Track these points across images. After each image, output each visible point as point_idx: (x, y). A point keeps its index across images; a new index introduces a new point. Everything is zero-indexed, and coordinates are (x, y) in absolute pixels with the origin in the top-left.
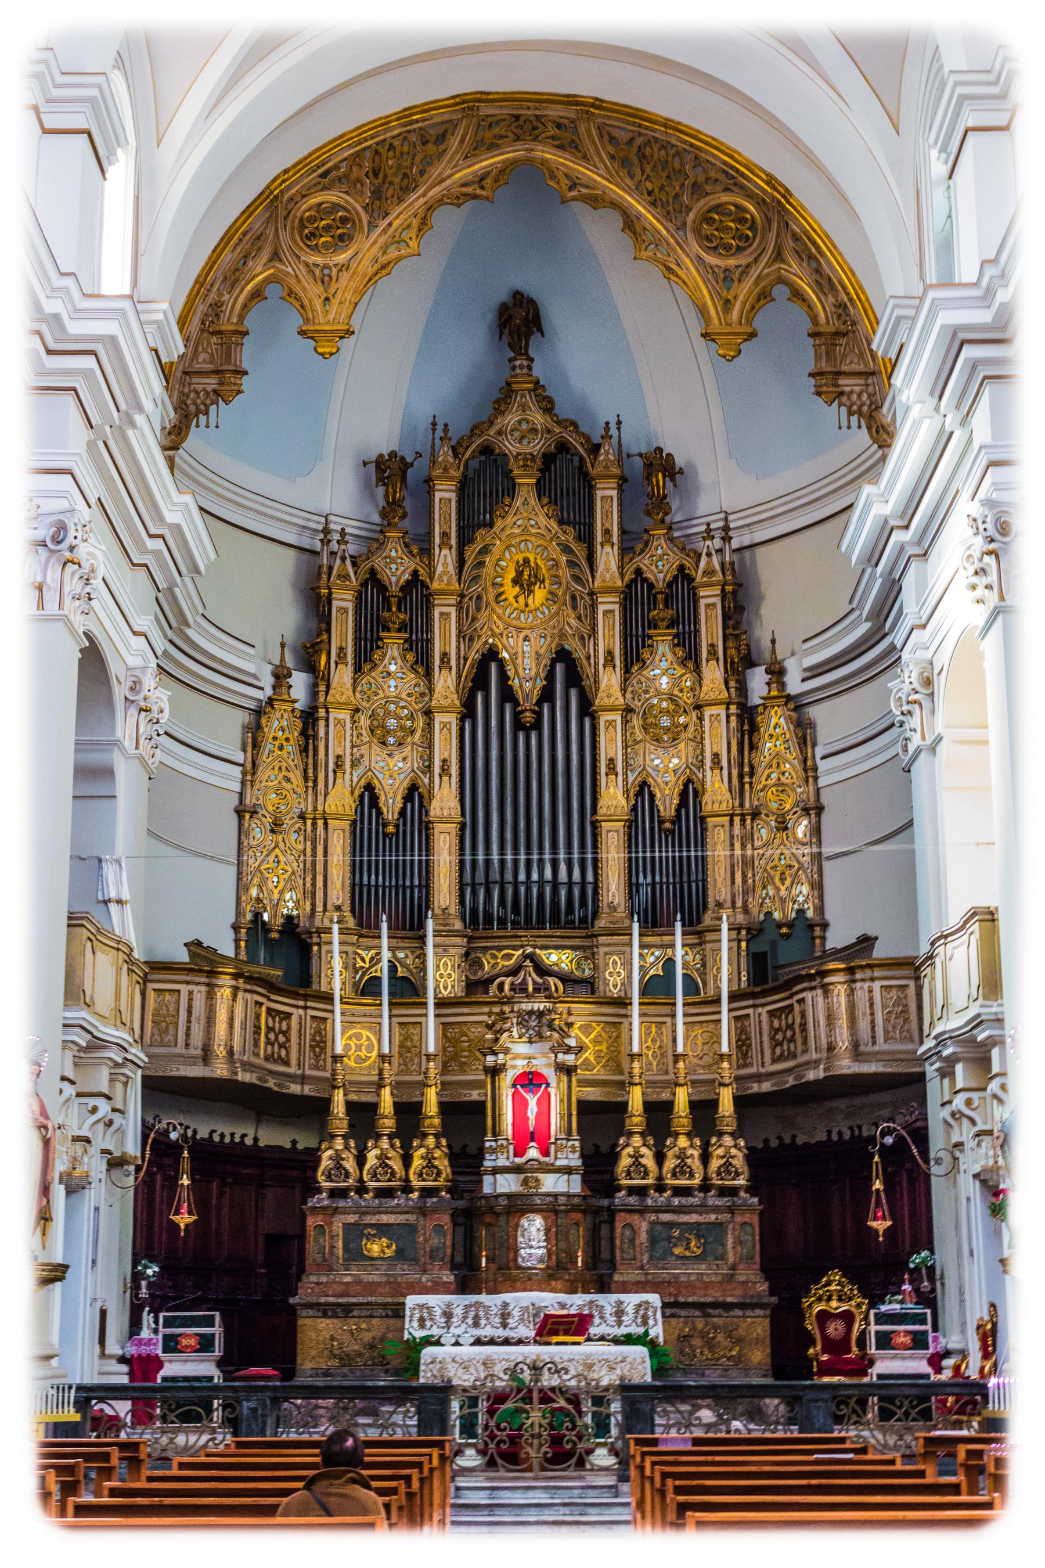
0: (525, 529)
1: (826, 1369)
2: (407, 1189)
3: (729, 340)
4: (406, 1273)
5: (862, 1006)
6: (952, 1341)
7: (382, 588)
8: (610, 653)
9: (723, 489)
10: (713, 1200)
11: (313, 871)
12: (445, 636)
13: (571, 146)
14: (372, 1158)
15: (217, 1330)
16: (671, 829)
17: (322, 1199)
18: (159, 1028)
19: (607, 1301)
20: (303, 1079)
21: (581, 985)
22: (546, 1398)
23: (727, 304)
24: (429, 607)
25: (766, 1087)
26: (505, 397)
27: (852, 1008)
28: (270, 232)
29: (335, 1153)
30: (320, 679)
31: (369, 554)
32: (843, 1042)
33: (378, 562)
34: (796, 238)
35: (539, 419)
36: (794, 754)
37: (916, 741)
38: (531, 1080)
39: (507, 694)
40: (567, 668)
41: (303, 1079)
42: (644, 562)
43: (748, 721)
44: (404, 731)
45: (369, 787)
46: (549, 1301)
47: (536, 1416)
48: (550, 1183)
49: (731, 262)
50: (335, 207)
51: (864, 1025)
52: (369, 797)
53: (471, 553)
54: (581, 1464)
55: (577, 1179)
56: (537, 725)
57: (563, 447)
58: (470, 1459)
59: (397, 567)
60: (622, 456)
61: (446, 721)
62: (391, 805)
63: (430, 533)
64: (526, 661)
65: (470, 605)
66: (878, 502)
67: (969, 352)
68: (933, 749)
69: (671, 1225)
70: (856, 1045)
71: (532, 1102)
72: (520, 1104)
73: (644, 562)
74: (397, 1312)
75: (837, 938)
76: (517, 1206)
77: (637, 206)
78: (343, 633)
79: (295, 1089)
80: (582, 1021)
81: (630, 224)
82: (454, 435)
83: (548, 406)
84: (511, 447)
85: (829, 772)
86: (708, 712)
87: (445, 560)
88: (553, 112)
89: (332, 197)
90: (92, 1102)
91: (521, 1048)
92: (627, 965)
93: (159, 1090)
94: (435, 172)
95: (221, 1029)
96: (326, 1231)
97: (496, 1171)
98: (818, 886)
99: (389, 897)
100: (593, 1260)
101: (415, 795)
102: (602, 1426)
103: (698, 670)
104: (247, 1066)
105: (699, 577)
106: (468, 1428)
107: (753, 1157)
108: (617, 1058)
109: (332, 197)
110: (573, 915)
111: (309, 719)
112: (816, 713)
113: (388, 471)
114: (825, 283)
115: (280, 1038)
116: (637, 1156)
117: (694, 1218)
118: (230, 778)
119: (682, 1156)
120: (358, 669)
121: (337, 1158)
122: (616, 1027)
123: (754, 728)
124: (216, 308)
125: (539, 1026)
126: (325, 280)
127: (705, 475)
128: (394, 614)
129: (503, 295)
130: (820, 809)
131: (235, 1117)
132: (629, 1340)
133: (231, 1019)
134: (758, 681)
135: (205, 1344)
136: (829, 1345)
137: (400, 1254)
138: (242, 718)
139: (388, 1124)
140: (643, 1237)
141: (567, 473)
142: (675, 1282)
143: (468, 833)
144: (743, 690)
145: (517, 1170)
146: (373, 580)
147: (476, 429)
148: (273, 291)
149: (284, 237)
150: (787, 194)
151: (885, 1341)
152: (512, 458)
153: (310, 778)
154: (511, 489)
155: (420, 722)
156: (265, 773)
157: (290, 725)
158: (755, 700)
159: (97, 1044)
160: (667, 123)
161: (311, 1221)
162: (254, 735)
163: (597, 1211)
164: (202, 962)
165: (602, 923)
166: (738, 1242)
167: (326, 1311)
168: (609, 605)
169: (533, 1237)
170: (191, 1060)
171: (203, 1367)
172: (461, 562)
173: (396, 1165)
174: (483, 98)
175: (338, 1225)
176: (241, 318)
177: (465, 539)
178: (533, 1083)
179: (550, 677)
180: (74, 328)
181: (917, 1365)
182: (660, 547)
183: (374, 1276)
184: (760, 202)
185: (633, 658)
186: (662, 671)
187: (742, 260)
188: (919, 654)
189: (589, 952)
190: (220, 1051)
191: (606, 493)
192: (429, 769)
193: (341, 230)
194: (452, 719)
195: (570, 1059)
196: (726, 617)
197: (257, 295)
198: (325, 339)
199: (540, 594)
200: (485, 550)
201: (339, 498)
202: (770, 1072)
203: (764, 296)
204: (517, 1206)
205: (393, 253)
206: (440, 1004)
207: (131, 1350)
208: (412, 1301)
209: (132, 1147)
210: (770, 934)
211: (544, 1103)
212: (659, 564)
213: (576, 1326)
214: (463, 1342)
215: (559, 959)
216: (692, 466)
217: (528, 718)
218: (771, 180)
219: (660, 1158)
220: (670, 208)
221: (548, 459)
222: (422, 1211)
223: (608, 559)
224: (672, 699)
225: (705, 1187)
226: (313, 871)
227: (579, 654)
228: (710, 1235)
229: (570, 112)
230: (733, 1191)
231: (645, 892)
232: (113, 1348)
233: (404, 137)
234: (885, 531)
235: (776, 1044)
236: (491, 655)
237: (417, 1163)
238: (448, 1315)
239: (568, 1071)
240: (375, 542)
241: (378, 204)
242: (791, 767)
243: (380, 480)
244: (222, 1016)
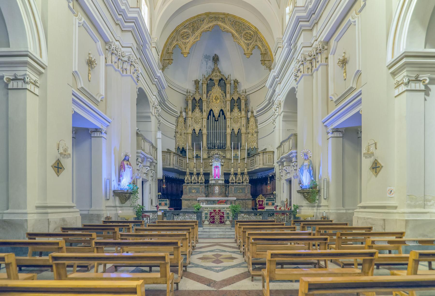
0: (216, 91)
1: (259, 209)
2: (198, 183)
3: (248, 55)
6: (279, 204)
8: (228, 110)
9: (245, 85)
11: (186, 140)
12: (205, 107)
13: (224, 22)
14: (193, 178)
16: (237, 136)
17: (186, 184)
24: (202, 103)
27: (263, 158)
28: (176, 36)
29: (187, 178)
30: (187, 113)
34: (259, 38)
35: (218, 74)
38: (217, 167)
39: (214, 116)
43: (248, 120)
44: (198, 122)
48: (220, 182)
49: (249, 42)
50: (187, 32)
53: (208, 95)
55: (223, 181)
56: (218, 120)
57: (222, 79)
58: (206, 222)
61: (205, 120)
62: (197, 132)
64: (216, 112)
67: (301, 23)
69: (237, 188)
71: (217, 170)
76: (214, 185)
77: (234, 32)
81: (233, 35)
83: (220, 72)
85: (260, 127)
86: (242, 118)
88: (221, 16)
90: (147, 167)
95: (172, 161)
97: (211, 180)
98: (257, 143)
102: (228, 217)
105: (241, 98)
111: (185, 119)
112: (257, 118)
113: (197, 82)
114: (263, 46)
117: (241, 187)
119: (239, 178)
120: (192, 112)
121: (188, 178)
128: (197, 104)
133: (173, 160)
134: (249, 114)
135: (166, 204)
136: (260, 205)
137: (197, 192)
140: (233, 190)
141: (222, 82)
144: (247, 115)
146: (194, 99)
149: (179, 37)
150: (258, 30)
151: (267, 204)
153: (185, 128)
155: (201, 120)
156: (179, 127)
158: (249, 117)
160: (239, 18)
162: (177, 122)
166: (247, 190)
167: (186, 200)
168: (228, 103)
174: (210, 13)
175: (188, 187)
176: (172, 51)
178: (217, 169)
179: (220, 113)
181: (272, 208)
182: (236, 94)
187: (250, 42)
191: (228, 86)
194: (206, 119)
195: (223, 164)
199: (218, 101)
200: (211, 94)
203: (254, 48)
204: (214, 185)
210: (250, 150)
217: (217, 119)
219: (236, 178)
220: (239, 32)
221: (220, 80)
222: (200, 186)
227: (224, 110)
229: (223, 16)
236: (211, 110)
237: (200, 179)
242: (254, 127)
243: (195, 84)
244: (172, 159)
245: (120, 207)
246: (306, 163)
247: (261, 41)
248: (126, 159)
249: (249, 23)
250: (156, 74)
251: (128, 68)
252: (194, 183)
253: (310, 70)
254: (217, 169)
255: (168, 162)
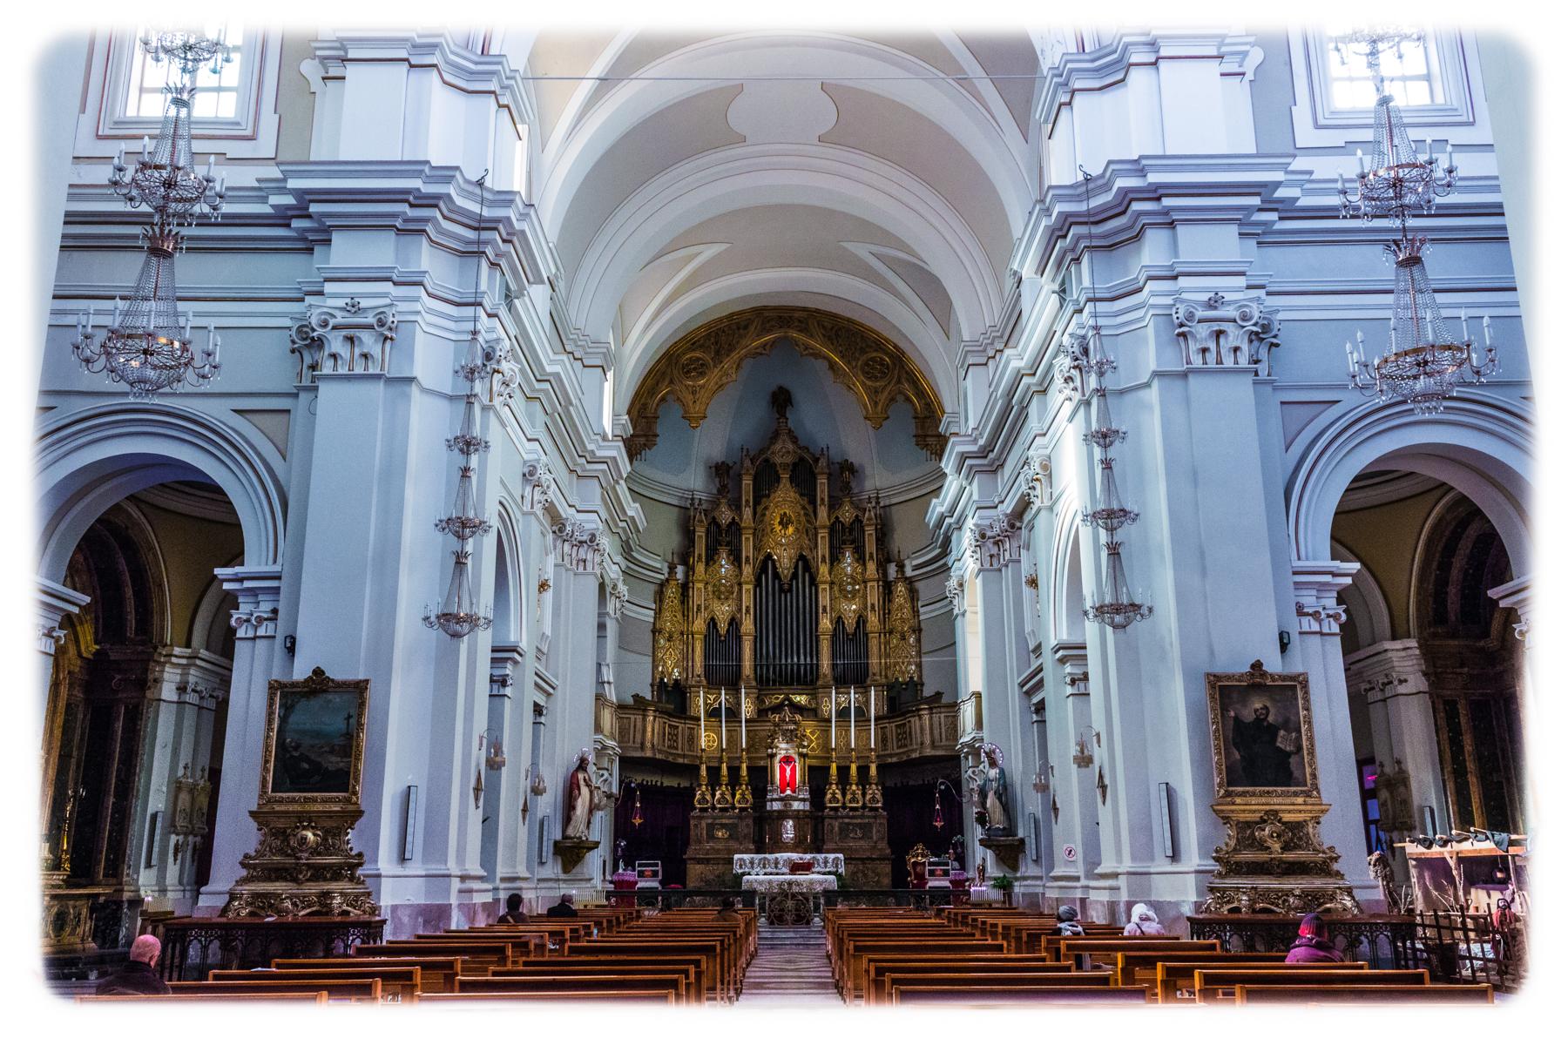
0: (784, 499)
2: (734, 808)
3: (877, 420)
4: (733, 844)
5: (936, 725)
7: (718, 526)
9: (878, 479)
10: (867, 813)
11: (687, 657)
12: (747, 549)
13: (804, 330)
15: (659, 868)
16: (851, 639)
17: (696, 813)
18: (623, 735)
19: (820, 857)
20: (684, 756)
21: (812, 712)
22: (794, 896)
23: (876, 404)
25: (895, 760)
26: (775, 436)
30: (690, 570)
31: (713, 509)
32: (928, 741)
33: (716, 514)
35: (791, 447)
36: (908, 605)
37: (956, 611)
38: (787, 760)
39: (776, 575)
40: (804, 564)
41: (684, 756)
42: (839, 513)
43: (887, 589)
44: (727, 594)
45: (713, 619)
46: (795, 856)
47: (790, 904)
48: (796, 805)
50: (698, 359)
51: (936, 732)
52: (712, 623)
53: (759, 509)
54: (808, 923)
56: (790, 590)
57: (802, 459)
59: (725, 516)
60: (830, 463)
61: (748, 587)
62: (723, 627)
63: (740, 497)
64: (784, 559)
65: (760, 534)
66: (938, 506)
68: (963, 614)
70: (933, 742)
72: (783, 771)
73: (839, 513)
74: (730, 861)
75: (928, 691)
76: (783, 815)
78: (700, 548)
79: (680, 760)
80: (809, 728)
81: (832, 366)
82: (752, 453)
83: (795, 440)
84: (778, 460)
87: (747, 513)
88: (796, 315)
89: (698, 354)
91: (783, 746)
92: (831, 704)
93: (627, 763)
94: (744, 342)
95: (649, 734)
96: (698, 828)
98: (919, 666)
99: (723, 675)
100: (814, 840)
101: (734, 623)
102: (817, 908)
103: (864, 564)
104: (660, 751)
106: (762, 908)
107: (886, 793)
108: (826, 746)
109: (698, 354)
110: (808, 679)
112: (920, 586)
114: (921, 394)
115: (674, 737)
116: (834, 794)
118: (648, 616)
119: (854, 793)
120: (707, 564)
121: (703, 794)
122: (826, 732)
123: (890, 592)
124: (645, 406)
125: (791, 736)
126: (694, 393)
127: (868, 471)
128: (724, 539)
129: (774, 387)
130: (920, 630)
131: (654, 773)
132: (829, 873)
134: (892, 570)
135: (655, 874)
138: (653, 588)
139: (725, 780)
142: (850, 848)
143: (758, 640)
144: (885, 574)
145: (781, 799)
146: (714, 521)
147: (762, 451)
148: (670, 398)
150: (903, 353)
151: (932, 873)
152: (779, 463)
154: (778, 480)
155: (736, 589)
156: (667, 615)
157: (673, 592)
159: (605, 748)
160: (849, 320)
161: (692, 822)
162: (660, 596)
163: (816, 818)
164: (639, 704)
165: (820, 683)
167: (699, 861)
168: (823, 534)
169: (789, 830)
170: (635, 749)
171: (654, 884)
172: (755, 513)
173: (729, 797)
177: (757, 503)
178: (787, 760)
179: (796, 567)
180: (598, 453)
183: (720, 846)
184: (891, 356)
185: (835, 559)
186: (848, 562)
188: (1041, 452)
189: (813, 696)
190: (649, 745)
191: (822, 481)
192: (740, 610)
193: (701, 369)
194: (751, 587)
196: (878, 540)
197: (663, 399)
198: (692, 420)
199: (791, 529)
200: (766, 508)
201: (696, 481)
202: (895, 755)
204: (783, 815)
205: (724, 380)
206: (747, 721)
207: (615, 878)
208: (736, 857)
209: (615, 790)
211: (793, 770)
212: (847, 514)
213: (807, 867)
214: (761, 872)
215: (801, 699)
216: (862, 466)
218: (895, 346)
219: (844, 795)
221: (795, 465)
223: (823, 512)
224: (852, 577)
225: (864, 806)
226: (687, 657)
228: (865, 828)
229: (805, 314)
230: (876, 809)
231: (839, 669)
232: (608, 877)
233: (729, 327)
234: (942, 518)
235: (899, 740)
236: (769, 556)
238: (752, 863)
239: (802, 756)
240: (715, 504)
241: (719, 356)
242: (907, 613)
245: (565, 881)
246: (993, 773)
247: (915, 383)
248: (582, 765)
249: (877, 334)
250: (625, 513)
251: (590, 557)
252: (722, 810)
253: (995, 560)
254: (787, 760)
255: (639, 737)
